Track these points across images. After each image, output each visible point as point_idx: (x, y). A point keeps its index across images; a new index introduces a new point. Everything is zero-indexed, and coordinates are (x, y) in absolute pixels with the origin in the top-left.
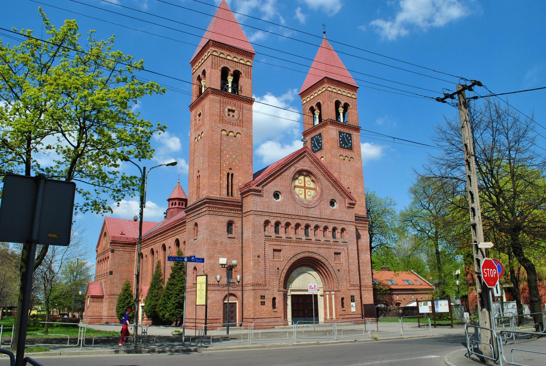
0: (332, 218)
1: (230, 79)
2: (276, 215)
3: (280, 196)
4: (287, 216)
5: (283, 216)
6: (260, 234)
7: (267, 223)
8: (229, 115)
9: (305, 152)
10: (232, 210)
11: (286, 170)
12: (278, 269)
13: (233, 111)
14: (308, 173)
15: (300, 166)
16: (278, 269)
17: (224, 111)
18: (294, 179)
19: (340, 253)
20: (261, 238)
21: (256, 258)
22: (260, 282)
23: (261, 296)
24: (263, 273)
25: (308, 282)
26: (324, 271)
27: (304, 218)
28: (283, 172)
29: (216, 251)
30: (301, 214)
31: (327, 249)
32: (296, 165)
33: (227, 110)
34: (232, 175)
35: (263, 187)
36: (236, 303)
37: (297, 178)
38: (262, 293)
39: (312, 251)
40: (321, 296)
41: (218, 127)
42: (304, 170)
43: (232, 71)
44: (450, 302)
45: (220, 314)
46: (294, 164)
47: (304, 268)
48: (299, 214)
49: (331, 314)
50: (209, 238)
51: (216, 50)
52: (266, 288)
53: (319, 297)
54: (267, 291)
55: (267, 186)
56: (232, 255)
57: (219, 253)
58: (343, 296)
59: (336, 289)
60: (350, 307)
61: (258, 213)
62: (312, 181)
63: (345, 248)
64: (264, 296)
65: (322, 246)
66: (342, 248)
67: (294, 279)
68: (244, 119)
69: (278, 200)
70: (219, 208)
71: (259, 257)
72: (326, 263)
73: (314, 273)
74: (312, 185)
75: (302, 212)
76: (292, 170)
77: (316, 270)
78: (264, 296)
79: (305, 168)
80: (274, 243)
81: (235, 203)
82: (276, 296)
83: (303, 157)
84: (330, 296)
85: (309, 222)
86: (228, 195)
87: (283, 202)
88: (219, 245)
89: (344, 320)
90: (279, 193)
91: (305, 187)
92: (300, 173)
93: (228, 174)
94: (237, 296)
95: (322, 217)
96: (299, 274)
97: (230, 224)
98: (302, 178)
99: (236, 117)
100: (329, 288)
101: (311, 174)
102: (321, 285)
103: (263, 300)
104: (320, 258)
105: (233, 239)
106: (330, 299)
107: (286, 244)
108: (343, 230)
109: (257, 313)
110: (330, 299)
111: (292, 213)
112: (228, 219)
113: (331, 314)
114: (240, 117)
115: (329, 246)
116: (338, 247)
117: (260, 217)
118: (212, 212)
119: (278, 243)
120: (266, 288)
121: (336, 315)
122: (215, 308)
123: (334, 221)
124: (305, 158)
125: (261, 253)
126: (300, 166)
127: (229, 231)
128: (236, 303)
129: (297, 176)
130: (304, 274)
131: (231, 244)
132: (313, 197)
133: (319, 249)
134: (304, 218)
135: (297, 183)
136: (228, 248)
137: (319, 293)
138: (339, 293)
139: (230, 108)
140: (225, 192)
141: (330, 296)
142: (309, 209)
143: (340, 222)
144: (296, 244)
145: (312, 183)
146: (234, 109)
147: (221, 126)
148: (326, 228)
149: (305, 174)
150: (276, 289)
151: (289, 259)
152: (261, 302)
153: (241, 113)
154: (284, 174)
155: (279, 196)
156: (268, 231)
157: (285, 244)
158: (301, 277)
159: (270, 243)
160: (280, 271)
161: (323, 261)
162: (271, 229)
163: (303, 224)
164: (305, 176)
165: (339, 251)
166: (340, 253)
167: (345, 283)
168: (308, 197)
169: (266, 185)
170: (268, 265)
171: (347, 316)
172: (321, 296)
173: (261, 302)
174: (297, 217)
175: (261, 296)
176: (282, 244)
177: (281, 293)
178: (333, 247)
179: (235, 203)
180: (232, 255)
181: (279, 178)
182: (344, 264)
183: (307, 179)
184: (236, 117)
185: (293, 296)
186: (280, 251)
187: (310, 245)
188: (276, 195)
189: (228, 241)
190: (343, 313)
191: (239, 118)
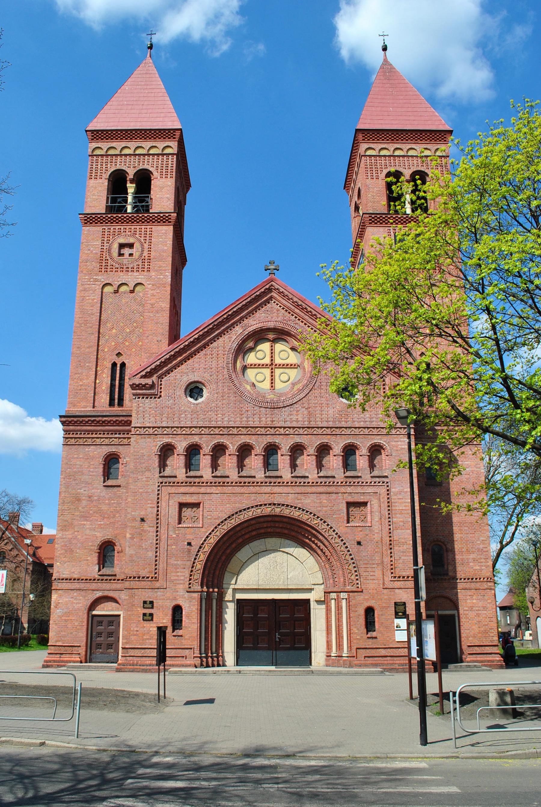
0: (343, 424)
1: (131, 188)
2: (188, 431)
3: (205, 390)
4: (217, 431)
5: (207, 431)
6: (147, 474)
7: (166, 451)
8: (120, 255)
9: (270, 290)
10: (116, 432)
11: (220, 335)
12: (189, 544)
13: (131, 246)
14: (281, 334)
15: (254, 323)
16: (189, 544)
17: (109, 250)
18: (242, 350)
19: (365, 504)
20: (151, 482)
21: (138, 523)
22: (143, 573)
23: (145, 602)
24: (151, 554)
25: (276, 572)
26: (322, 547)
27: (263, 431)
28: (213, 340)
29: (77, 513)
30: (257, 424)
31: (324, 496)
32: (246, 321)
33: (116, 246)
34: (123, 365)
35: (160, 377)
36: (119, 616)
37: (251, 349)
38: (148, 595)
39: (282, 501)
40: (318, 602)
41: (96, 280)
42: (269, 330)
43: (131, 173)
44: (408, 619)
45: (80, 637)
46: (242, 319)
47: (271, 542)
48: (251, 424)
49: (339, 646)
50: (64, 489)
51: (167, 144)
52: (157, 585)
53: (313, 605)
54: (159, 593)
55: (172, 374)
56: (112, 520)
57: (82, 516)
58: (371, 603)
59: (349, 588)
60: (392, 629)
61: (154, 431)
62: (293, 349)
63: (382, 491)
64: (152, 603)
65: (309, 490)
66: (370, 490)
67: (243, 566)
68: (153, 254)
69: (200, 400)
70: (89, 432)
71: (143, 520)
72: (322, 527)
73: (301, 552)
74: (293, 358)
75: (264, 418)
76: (238, 333)
77: (303, 545)
78: (152, 603)
79: (271, 325)
80: (182, 490)
81: (120, 419)
82: (180, 602)
83: (267, 302)
84: (338, 601)
85: (277, 440)
86: (111, 404)
87: (207, 403)
88: (84, 503)
89: (370, 661)
90: (200, 386)
91: (272, 366)
92: (259, 336)
93: (114, 365)
94: (120, 601)
95: (313, 424)
96: (257, 556)
97: (111, 462)
98: (265, 347)
99: (136, 255)
100: (335, 584)
101: (289, 334)
102: (319, 578)
103: (148, 611)
104: (304, 517)
105: (115, 489)
106: (339, 609)
107: (213, 490)
108: (376, 451)
109: (133, 638)
110: (339, 609)
111: (232, 424)
112: (106, 450)
113: (339, 646)
114: (145, 254)
115: (333, 489)
116: (359, 490)
117: (149, 440)
118: (81, 441)
119: (193, 489)
120: (157, 585)
121: (350, 647)
122: (69, 626)
123: (348, 431)
124: (272, 305)
125: (150, 512)
126: (254, 323)
127: (107, 473)
128: (119, 616)
129: (251, 344)
130: (273, 555)
131: (110, 499)
132: (293, 384)
133: (300, 496)
134: (263, 431)
135: (251, 358)
136: (104, 508)
137: (312, 596)
138: (359, 597)
139: (122, 241)
140: (104, 398)
141: (338, 601)
142: (276, 411)
143: (366, 431)
144: (238, 489)
145: (292, 354)
146: (131, 240)
147: (103, 278)
148: (323, 450)
149: (271, 336)
150: (181, 589)
151: (218, 522)
152: (144, 615)
153: (146, 246)
154: (215, 344)
155: (202, 390)
156: (172, 466)
157: (209, 490)
158: (264, 561)
159: (173, 490)
160: (195, 549)
161: (314, 522)
162: (176, 464)
163: (259, 445)
164: (274, 341)
165: (361, 499)
166: (365, 504)
167: (378, 573)
168: (278, 385)
169: (168, 372)
170: (164, 537)
171: (383, 652)
172: (318, 602)
173: (144, 615)
174: (244, 431)
175: (145, 602)
176: (203, 490)
177: (196, 595)
178: (342, 490)
179: (120, 419)
180: (112, 520)
181: (202, 353)
182: (376, 527)
183: (279, 347)
184: (136, 255)
185: (241, 604)
186: (197, 505)
187: (276, 489)
188: (194, 390)
189: (105, 493)
190: (370, 643)
191: (141, 256)
